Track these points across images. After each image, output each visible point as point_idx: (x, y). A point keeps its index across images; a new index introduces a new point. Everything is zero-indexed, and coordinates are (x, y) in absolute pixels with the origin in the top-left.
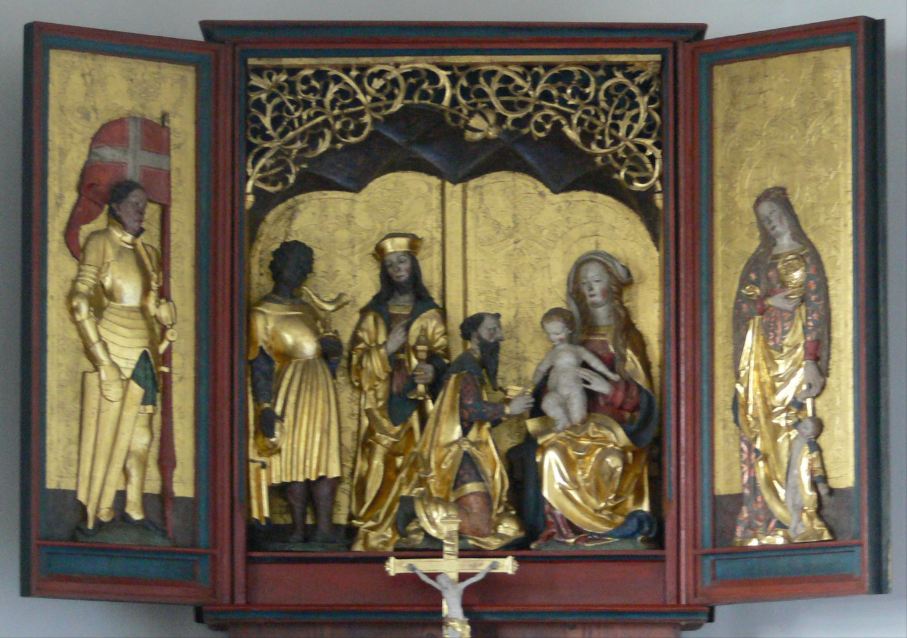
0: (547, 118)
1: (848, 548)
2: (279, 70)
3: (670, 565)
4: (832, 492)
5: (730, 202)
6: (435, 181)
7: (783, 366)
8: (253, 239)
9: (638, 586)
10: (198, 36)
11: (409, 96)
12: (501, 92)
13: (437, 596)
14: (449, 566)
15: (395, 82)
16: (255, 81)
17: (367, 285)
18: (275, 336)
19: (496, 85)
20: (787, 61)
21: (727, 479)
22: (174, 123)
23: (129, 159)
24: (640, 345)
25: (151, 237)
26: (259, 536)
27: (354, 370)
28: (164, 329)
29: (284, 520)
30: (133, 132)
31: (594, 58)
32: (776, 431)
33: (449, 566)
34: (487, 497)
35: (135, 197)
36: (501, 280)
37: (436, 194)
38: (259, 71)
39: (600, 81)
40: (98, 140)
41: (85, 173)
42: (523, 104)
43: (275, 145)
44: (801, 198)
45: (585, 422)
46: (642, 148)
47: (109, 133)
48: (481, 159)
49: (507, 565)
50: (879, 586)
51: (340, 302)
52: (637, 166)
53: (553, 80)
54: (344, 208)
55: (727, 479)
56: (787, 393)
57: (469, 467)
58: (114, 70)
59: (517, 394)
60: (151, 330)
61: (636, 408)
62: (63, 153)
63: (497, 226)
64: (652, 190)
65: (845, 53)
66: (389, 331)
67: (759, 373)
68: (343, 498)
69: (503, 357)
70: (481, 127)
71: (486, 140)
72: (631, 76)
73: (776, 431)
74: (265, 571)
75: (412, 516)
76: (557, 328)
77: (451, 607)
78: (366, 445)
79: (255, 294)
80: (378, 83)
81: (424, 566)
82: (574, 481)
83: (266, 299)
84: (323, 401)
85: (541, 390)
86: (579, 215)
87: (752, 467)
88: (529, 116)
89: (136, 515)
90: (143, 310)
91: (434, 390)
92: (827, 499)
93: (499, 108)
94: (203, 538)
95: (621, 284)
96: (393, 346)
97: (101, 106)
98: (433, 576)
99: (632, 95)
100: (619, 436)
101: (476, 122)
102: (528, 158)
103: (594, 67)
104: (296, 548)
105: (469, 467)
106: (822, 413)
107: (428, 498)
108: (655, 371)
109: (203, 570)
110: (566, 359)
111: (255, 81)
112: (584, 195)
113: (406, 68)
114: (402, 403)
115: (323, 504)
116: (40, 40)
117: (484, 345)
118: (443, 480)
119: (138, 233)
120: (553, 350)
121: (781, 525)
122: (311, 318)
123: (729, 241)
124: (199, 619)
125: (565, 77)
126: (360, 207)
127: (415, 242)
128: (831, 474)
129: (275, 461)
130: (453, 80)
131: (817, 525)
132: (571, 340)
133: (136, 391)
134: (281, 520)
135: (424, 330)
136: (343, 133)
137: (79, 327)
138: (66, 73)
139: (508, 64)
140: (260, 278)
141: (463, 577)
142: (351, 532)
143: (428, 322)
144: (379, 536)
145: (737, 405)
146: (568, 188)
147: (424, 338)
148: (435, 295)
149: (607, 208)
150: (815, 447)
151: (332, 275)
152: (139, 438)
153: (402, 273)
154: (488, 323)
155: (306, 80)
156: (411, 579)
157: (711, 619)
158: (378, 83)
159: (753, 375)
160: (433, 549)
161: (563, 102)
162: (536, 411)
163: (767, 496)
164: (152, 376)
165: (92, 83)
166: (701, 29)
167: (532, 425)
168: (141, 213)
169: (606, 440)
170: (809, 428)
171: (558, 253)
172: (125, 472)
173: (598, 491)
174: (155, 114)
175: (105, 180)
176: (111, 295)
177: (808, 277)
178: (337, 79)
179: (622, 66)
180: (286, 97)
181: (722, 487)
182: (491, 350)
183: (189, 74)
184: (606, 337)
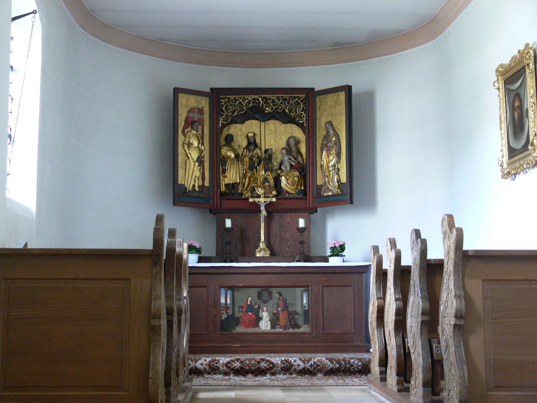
0: (282, 108)
1: (345, 195)
2: (226, 98)
3: (308, 200)
4: (341, 183)
5: (320, 124)
6: (259, 122)
7: (331, 158)
8: (221, 134)
9: (301, 204)
10: (210, 91)
11: (253, 103)
12: (272, 102)
13: (260, 206)
14: (262, 200)
15: (250, 101)
16: (221, 100)
17: (245, 143)
18: (226, 153)
19: (271, 101)
20: (331, 95)
21: (319, 182)
22: (205, 109)
23: (195, 116)
24: (301, 155)
25: (200, 132)
26: (222, 194)
27: (242, 161)
28: (203, 151)
29: (228, 192)
30: (196, 110)
31: (292, 95)
32: (330, 171)
33: (262, 200)
34: (270, 186)
35: (196, 124)
36: (272, 142)
37: (259, 125)
38: (222, 98)
39: (293, 100)
40: (189, 112)
41: (186, 119)
42: (277, 105)
43: (225, 114)
44: (335, 123)
45: (290, 171)
46: (302, 114)
47: (191, 110)
48: (268, 117)
49: (274, 200)
50: (351, 202)
51: (239, 146)
52: (301, 118)
53: (283, 100)
54: (240, 127)
55: (320, 181)
56: (332, 163)
57: (266, 180)
58: (192, 98)
59: (276, 164)
60: (200, 152)
61: (301, 168)
62: (182, 114)
63: (272, 131)
64: (304, 122)
65: (344, 92)
66: (249, 152)
67: (326, 159)
68: (240, 187)
69: (273, 158)
70: (268, 110)
71: (269, 113)
72: (299, 99)
73: (330, 171)
74: (223, 201)
75: (255, 190)
76: (284, 151)
77: (263, 208)
78: (245, 176)
79: (222, 145)
80: (247, 101)
81: (257, 200)
82: (288, 183)
83: (224, 146)
85: (281, 164)
86: (289, 129)
87: (325, 179)
88: (278, 108)
89: (197, 190)
90: (198, 147)
91: (259, 164)
92: (340, 185)
93: (272, 106)
94: (211, 195)
95: (297, 142)
96: (250, 155)
97: (189, 105)
98: (259, 202)
99: (299, 103)
100: (297, 173)
101: (267, 109)
102: (278, 117)
103: (291, 97)
104: (230, 197)
106: (339, 167)
107: (257, 186)
108: (305, 161)
109: (211, 202)
110: (286, 158)
111: (221, 100)
112: (289, 124)
113: (253, 98)
114: (252, 167)
115: (236, 188)
116: (177, 91)
117: (269, 155)
118: (261, 182)
119: (197, 131)
120: (283, 156)
121: (331, 190)
122: (233, 150)
123: (320, 132)
124: (210, 212)
125: (286, 99)
126: (243, 127)
127: (255, 134)
128: (341, 180)
129: (226, 179)
130: (262, 100)
131: (338, 190)
132: (287, 154)
133: (197, 164)
134: (227, 192)
135: (256, 152)
136: (240, 111)
137: (185, 150)
138: (182, 98)
139: (274, 97)
140: (223, 142)
141: (265, 202)
142: (242, 194)
143: (258, 151)
144: (247, 194)
145: (322, 166)
146: (286, 123)
147: (256, 153)
148: (259, 145)
150: (338, 174)
151: (237, 141)
153: (252, 141)
154: (270, 150)
155: (232, 100)
156: (254, 203)
157: (316, 212)
158: (247, 101)
159: (325, 160)
160: (259, 196)
161: (285, 104)
162: (280, 168)
163: (328, 185)
164: (200, 161)
165: (188, 100)
166: (314, 89)
167: (279, 172)
168: (198, 127)
169: (294, 174)
170: (336, 170)
171: (284, 136)
172: (195, 180)
173: (293, 185)
174: (200, 107)
175: (190, 120)
176: (192, 144)
177: (336, 139)
178: (238, 100)
179: (297, 97)
180: (228, 104)
181: (318, 183)
182: (270, 156)
183: (208, 99)
184: (294, 153)
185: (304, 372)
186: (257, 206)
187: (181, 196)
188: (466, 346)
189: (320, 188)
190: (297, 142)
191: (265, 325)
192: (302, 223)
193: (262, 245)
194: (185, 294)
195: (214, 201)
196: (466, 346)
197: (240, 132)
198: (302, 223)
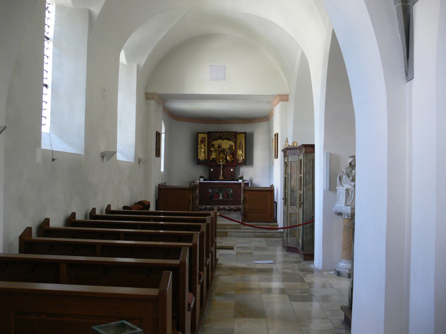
14: (221, 163)
17: (217, 146)
21: (237, 158)
26: (211, 161)
47: (202, 138)
57: (223, 157)
67: (240, 152)
84: (229, 214)
95: (232, 146)
105: (223, 157)
114: (219, 153)
116: (198, 133)
122: (214, 148)
138: (200, 135)
149: (231, 142)
152: (204, 155)
164: (204, 152)
185: (228, 210)
186: (220, 165)
187: (199, 162)
188: (244, 206)
189: (238, 160)
190: (232, 146)
191: (221, 198)
192: (232, 170)
193: (221, 176)
194: (198, 192)
195: (208, 163)
196: (244, 206)
197: (216, 143)
198: (232, 170)
